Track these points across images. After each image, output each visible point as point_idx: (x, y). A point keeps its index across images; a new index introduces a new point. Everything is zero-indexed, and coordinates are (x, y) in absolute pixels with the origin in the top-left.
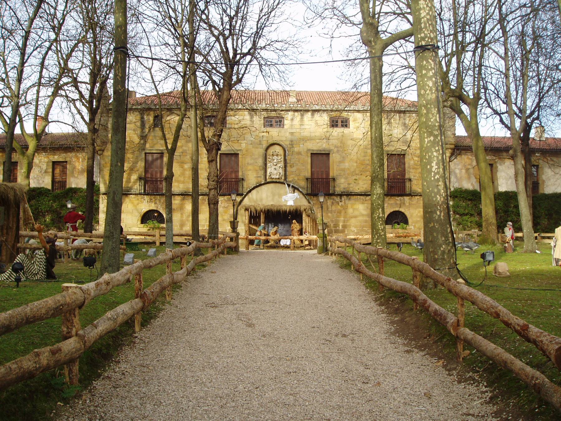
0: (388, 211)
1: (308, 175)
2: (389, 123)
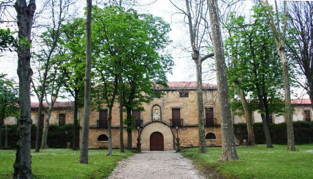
0: (206, 134)
1: (171, 118)
2: (206, 95)
